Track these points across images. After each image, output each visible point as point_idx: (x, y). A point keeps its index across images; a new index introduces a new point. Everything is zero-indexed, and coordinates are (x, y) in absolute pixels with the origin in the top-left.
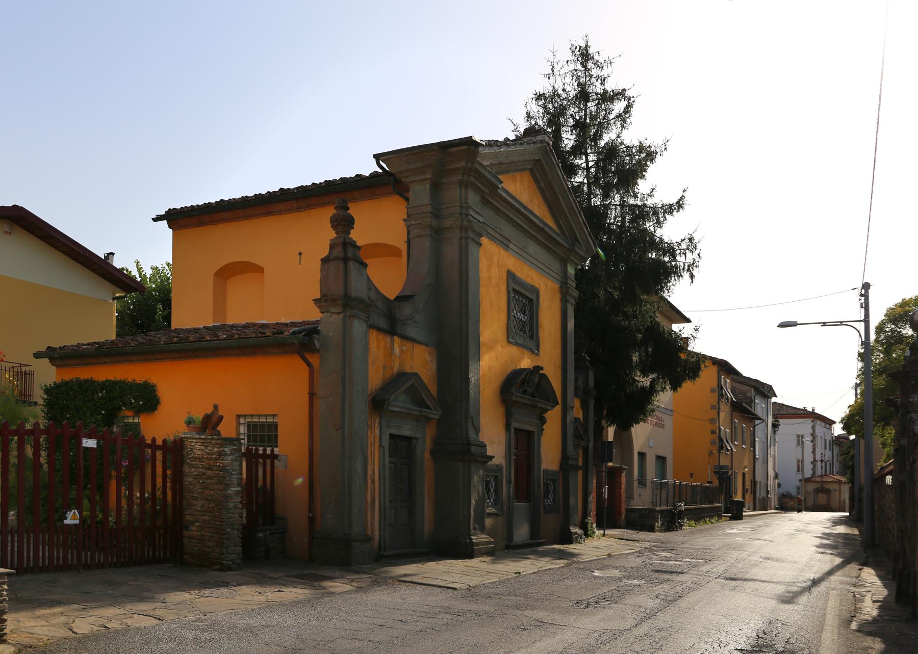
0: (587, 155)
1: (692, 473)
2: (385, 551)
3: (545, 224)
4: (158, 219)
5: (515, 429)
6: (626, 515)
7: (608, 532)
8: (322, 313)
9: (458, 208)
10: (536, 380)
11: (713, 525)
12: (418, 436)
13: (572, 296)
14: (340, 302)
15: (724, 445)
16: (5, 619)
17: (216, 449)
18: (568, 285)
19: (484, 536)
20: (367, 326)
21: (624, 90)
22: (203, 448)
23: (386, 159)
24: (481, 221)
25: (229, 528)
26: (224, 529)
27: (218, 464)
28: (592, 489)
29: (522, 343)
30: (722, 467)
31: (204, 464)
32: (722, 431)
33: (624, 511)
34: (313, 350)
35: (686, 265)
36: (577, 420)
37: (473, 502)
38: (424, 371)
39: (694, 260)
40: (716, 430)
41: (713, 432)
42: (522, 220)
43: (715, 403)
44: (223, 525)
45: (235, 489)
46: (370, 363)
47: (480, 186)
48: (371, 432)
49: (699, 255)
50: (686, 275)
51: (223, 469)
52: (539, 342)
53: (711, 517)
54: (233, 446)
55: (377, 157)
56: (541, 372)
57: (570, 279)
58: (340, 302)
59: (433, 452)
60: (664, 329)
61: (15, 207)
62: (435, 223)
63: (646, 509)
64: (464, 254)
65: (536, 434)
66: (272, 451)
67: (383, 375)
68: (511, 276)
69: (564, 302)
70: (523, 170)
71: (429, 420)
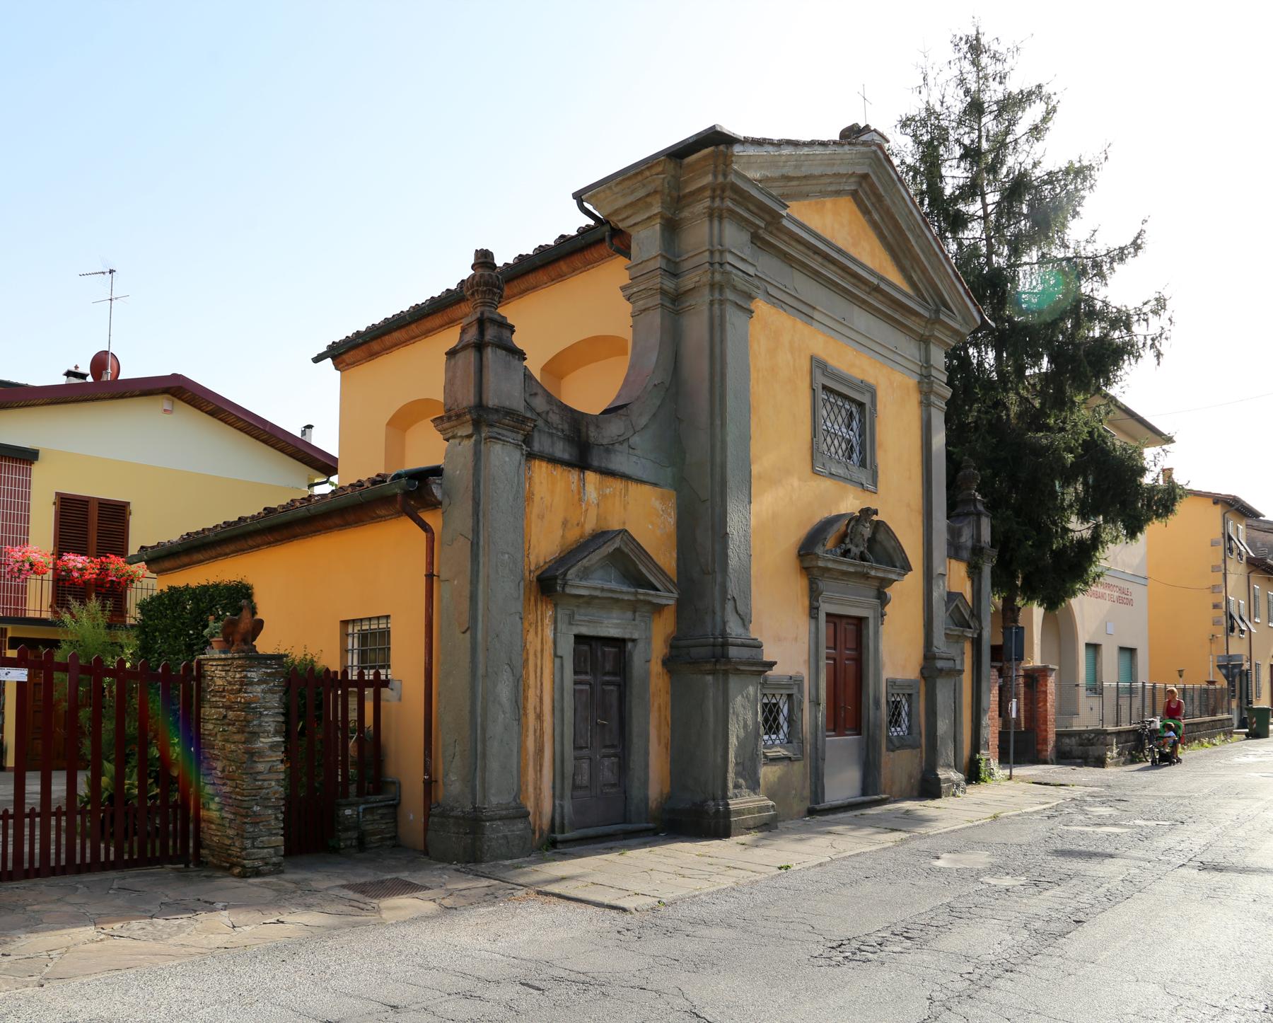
0: (983, 195)
1: (1182, 671)
2: (563, 832)
3: (882, 279)
4: (317, 359)
5: (829, 615)
6: (1057, 741)
7: (1019, 771)
8: (447, 440)
9: (707, 254)
10: (867, 532)
11: (1215, 749)
12: (635, 636)
13: (938, 395)
14: (468, 417)
15: (1236, 625)
17: (238, 676)
18: (932, 378)
19: (756, 798)
20: (522, 454)
21: (1039, 86)
22: (223, 673)
23: (591, 196)
24: (753, 274)
25: (257, 805)
26: (248, 808)
27: (239, 699)
28: (989, 704)
29: (842, 475)
30: (1230, 658)
31: (224, 700)
32: (1231, 603)
33: (1051, 738)
34: (435, 505)
35: (1149, 338)
36: (952, 597)
37: (733, 741)
39: (1163, 329)
40: (1221, 603)
41: (1216, 606)
43: (1220, 562)
44: (245, 801)
45: (270, 740)
46: (534, 517)
47: (746, 215)
48: (536, 633)
49: (1170, 319)
50: (1148, 355)
51: (247, 706)
52: (877, 472)
53: (1212, 736)
54: (266, 668)
55: (579, 197)
56: (875, 518)
57: (934, 368)
58: (468, 417)
59: (666, 662)
60: (1114, 445)
61: (175, 377)
62: (669, 285)
63: (1092, 731)
64: (717, 328)
65: (871, 622)
66: (377, 675)
67: (563, 536)
68: (818, 365)
69: (926, 404)
70: (838, 193)
71: (658, 609)
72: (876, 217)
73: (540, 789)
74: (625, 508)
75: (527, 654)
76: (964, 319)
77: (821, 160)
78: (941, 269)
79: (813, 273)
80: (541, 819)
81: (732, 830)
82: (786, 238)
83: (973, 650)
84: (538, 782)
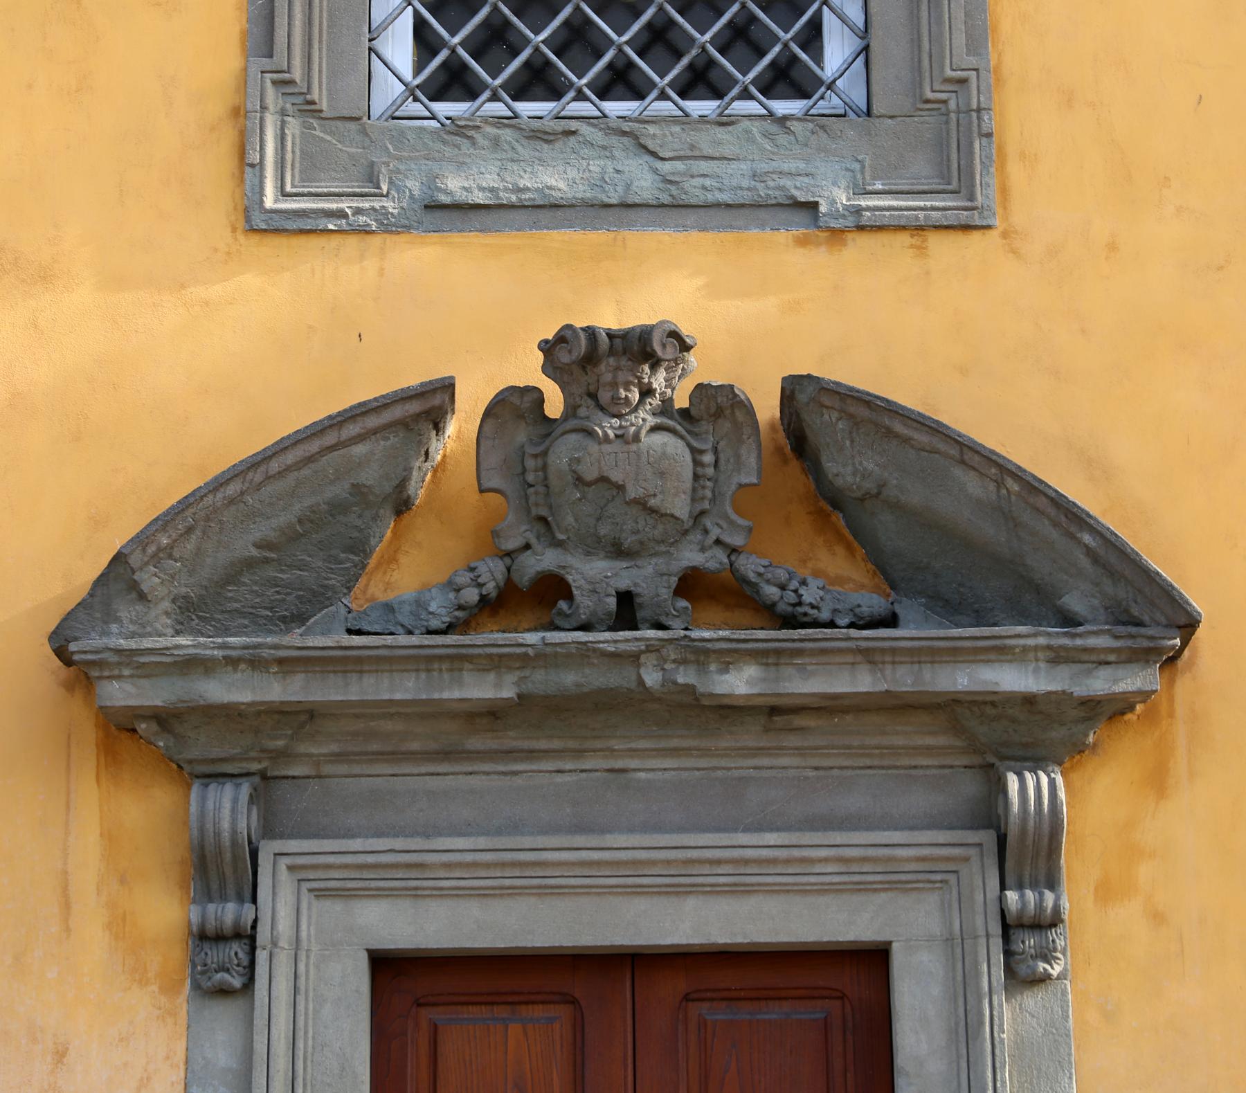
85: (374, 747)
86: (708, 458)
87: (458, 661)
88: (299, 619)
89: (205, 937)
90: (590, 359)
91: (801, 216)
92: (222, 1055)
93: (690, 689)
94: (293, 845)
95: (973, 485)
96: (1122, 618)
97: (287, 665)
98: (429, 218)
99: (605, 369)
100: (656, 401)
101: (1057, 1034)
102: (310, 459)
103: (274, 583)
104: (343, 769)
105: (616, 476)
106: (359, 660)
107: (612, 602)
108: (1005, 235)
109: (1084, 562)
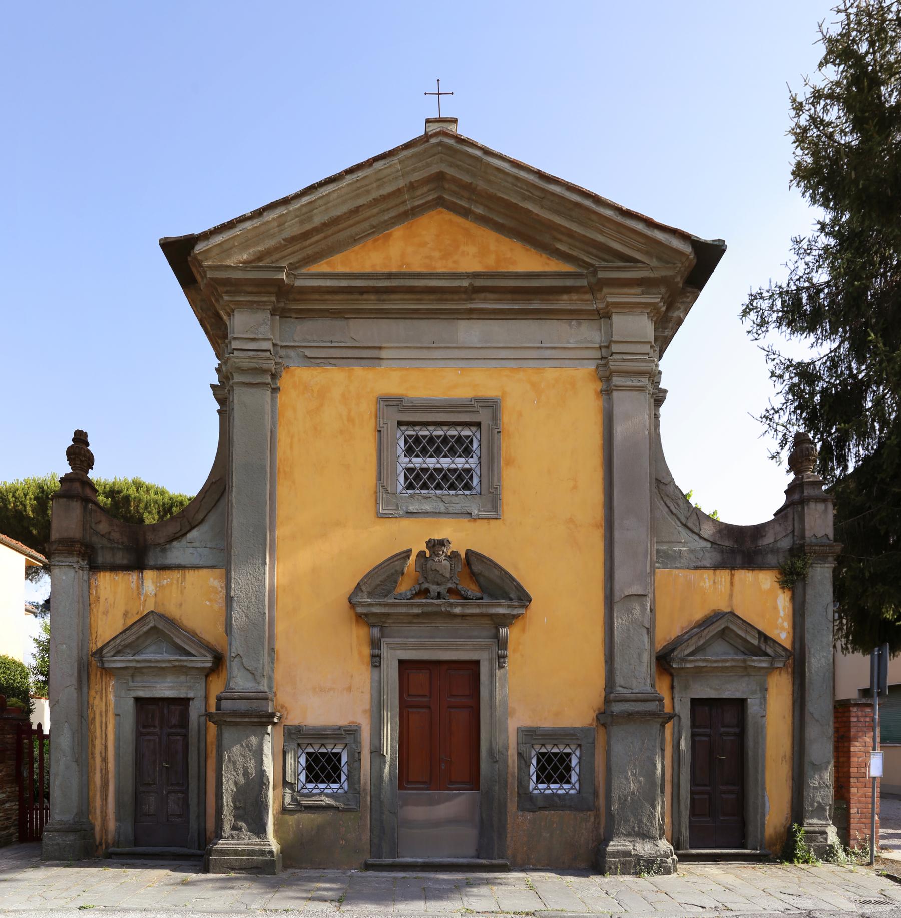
16: (794, 861)
38: (208, 603)
42: (413, 300)
48: (101, 698)
72: (479, 210)
73: (106, 813)
74: (182, 593)
75: (94, 714)
76: (659, 259)
77: (339, 197)
78: (594, 217)
79: (377, 313)
80: (106, 835)
81: (211, 867)
82: (317, 297)
83: (794, 684)
84: (104, 808)
85: (399, 621)
86: (453, 566)
87: (412, 605)
88: (386, 596)
89: (373, 656)
90: (434, 545)
91: (469, 516)
92: (376, 678)
93: (450, 611)
94: (386, 639)
95: (496, 572)
96: (520, 599)
97: (386, 605)
98: (408, 514)
99: (437, 546)
100: (445, 554)
101: (505, 674)
102: (389, 565)
103: (383, 589)
104: (394, 625)
105: (438, 569)
106: (397, 604)
107: (437, 594)
108: (503, 520)
109: (514, 588)
